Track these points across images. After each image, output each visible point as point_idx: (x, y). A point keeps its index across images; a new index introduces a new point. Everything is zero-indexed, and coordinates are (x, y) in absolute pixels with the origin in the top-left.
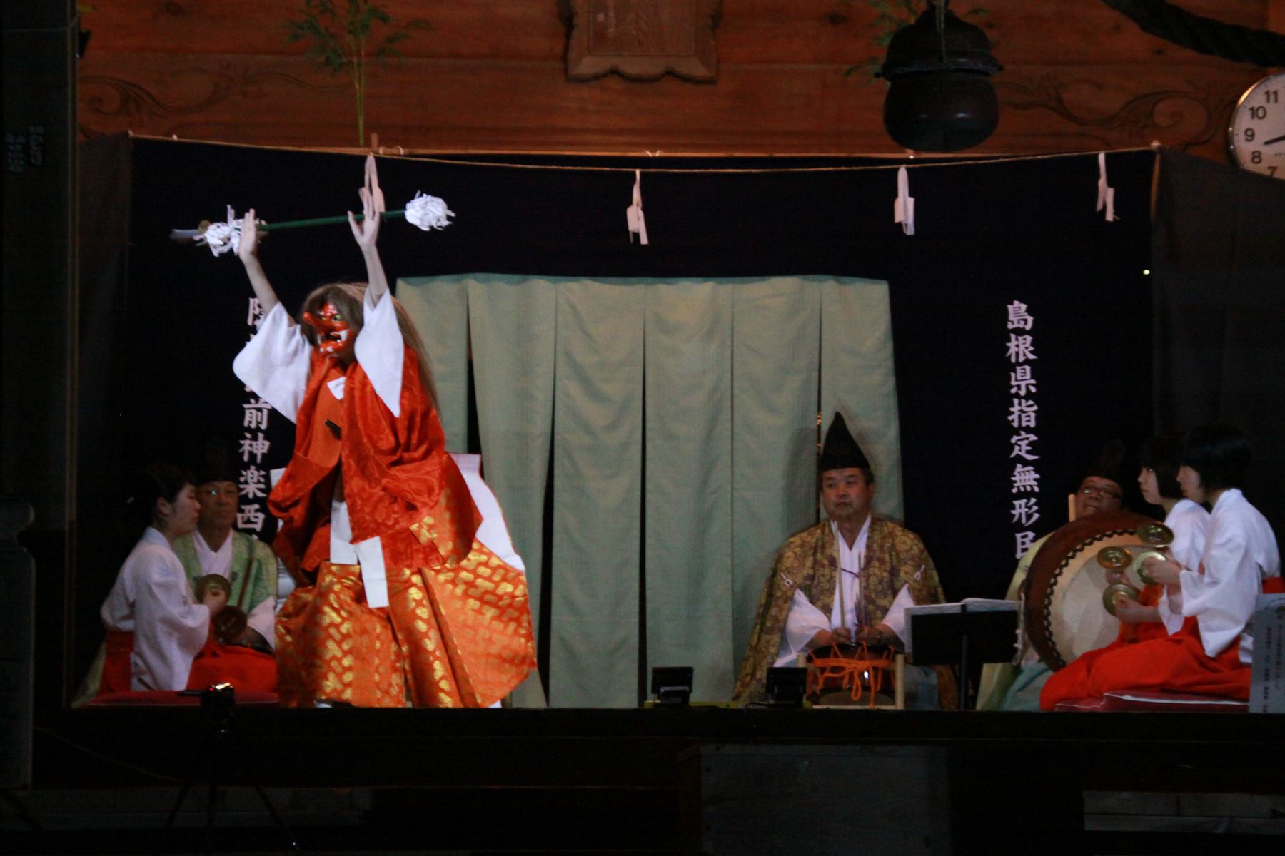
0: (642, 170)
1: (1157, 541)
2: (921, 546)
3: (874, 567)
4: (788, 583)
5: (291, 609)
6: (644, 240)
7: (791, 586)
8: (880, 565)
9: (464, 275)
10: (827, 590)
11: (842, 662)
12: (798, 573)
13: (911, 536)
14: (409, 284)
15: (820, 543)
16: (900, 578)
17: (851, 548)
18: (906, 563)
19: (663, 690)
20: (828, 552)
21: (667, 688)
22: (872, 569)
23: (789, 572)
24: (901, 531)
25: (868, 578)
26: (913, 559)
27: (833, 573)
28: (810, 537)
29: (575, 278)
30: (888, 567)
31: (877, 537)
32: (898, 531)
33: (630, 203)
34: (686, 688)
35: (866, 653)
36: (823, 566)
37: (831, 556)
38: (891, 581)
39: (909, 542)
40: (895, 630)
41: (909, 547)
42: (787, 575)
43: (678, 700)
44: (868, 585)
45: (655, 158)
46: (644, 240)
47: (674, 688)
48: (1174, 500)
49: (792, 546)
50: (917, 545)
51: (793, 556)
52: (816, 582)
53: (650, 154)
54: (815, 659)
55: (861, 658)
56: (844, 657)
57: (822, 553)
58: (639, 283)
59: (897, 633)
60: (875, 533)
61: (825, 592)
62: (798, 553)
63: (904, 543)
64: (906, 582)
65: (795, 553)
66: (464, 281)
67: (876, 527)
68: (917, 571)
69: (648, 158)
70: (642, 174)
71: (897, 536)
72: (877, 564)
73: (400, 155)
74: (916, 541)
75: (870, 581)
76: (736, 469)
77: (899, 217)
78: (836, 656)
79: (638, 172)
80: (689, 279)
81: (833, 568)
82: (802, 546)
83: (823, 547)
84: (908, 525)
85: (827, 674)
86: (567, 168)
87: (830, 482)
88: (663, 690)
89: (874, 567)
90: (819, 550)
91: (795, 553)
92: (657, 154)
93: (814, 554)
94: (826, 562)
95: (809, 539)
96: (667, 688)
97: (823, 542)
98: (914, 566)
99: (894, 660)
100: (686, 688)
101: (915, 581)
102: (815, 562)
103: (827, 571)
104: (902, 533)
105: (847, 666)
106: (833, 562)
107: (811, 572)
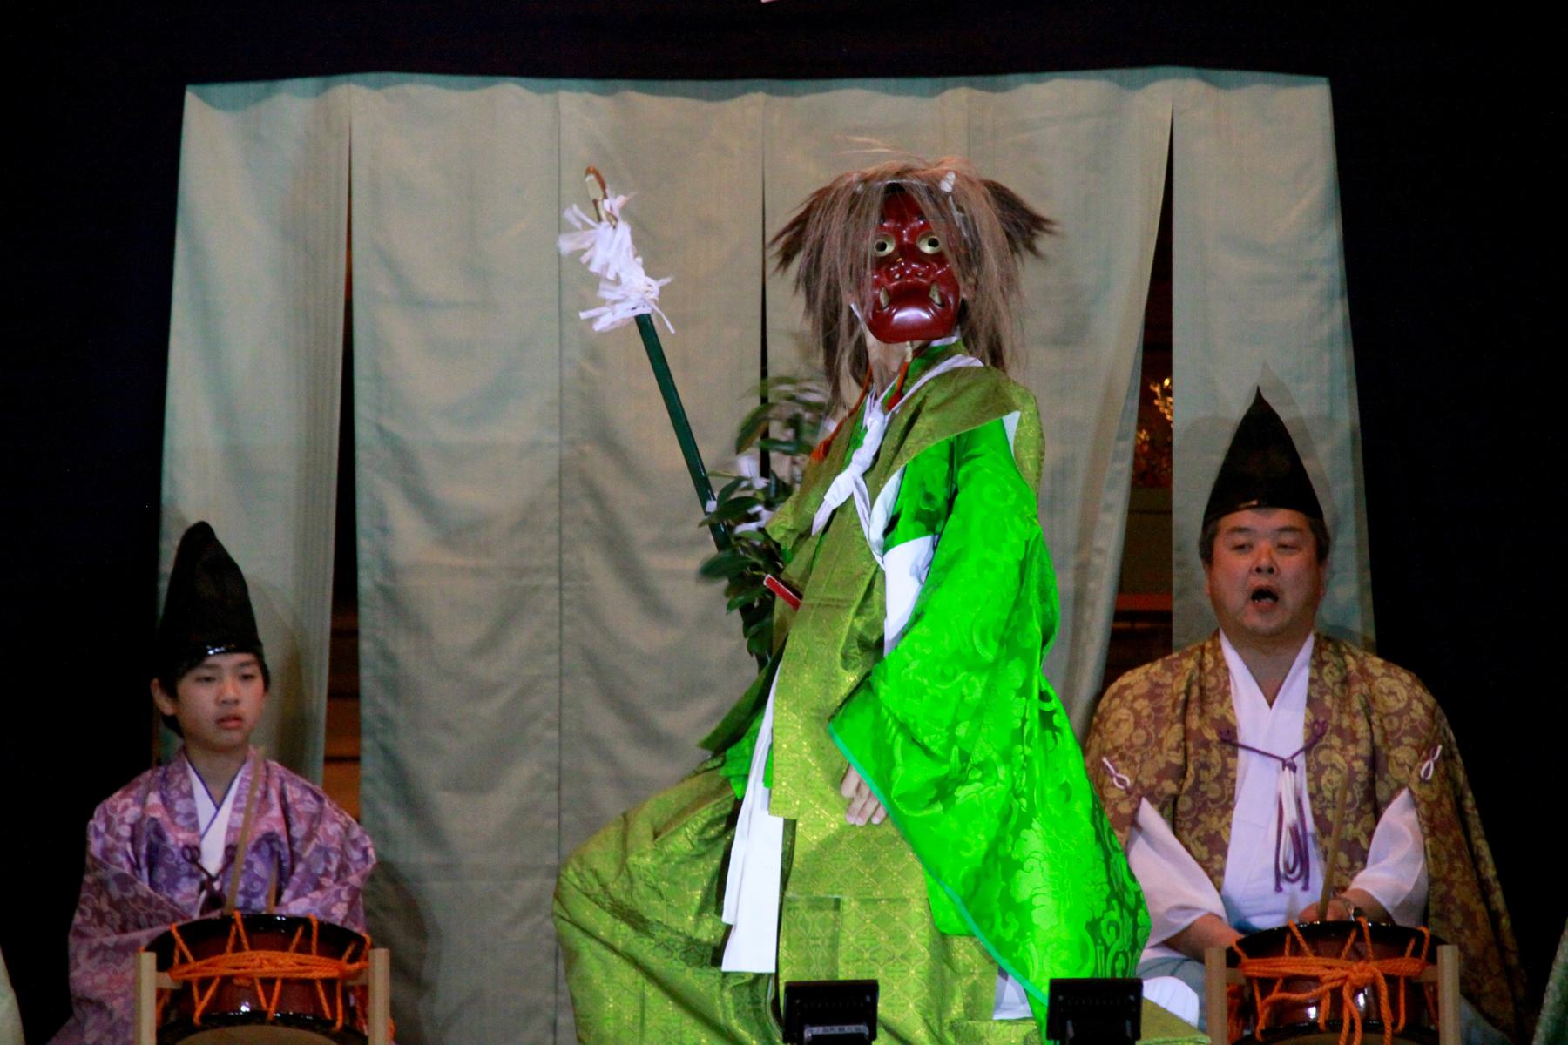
2: (1429, 700)
3: (1331, 747)
4: (1121, 781)
7: (1129, 792)
8: (89, 872)
10: (1213, 801)
11: (1310, 964)
12: (1142, 761)
13: (1406, 677)
15: (1195, 691)
16: (1387, 777)
17: (1271, 705)
18: (1399, 743)
20: (1217, 711)
21: (819, 1030)
22: (1325, 752)
23: (1122, 757)
24: (1383, 665)
25: (1316, 773)
26: (1413, 731)
27: (1230, 760)
28: (1169, 674)
30: (1364, 749)
31: (1330, 677)
32: (1375, 664)
34: (864, 1029)
35: (1368, 946)
36: (1206, 744)
37: (1224, 718)
38: (1372, 781)
39: (1403, 693)
40: (1384, 903)
41: (1402, 705)
42: (1119, 763)
44: (1319, 790)
48: (760, 716)
49: (1128, 695)
50: (1420, 700)
51: (1132, 719)
52: (1189, 782)
54: (1245, 959)
55: (1358, 955)
56: (1317, 954)
57: (1202, 713)
59: (1390, 910)
60: (1326, 670)
61: (1210, 804)
62: (1145, 713)
63: (1392, 693)
64: (1400, 787)
65: (1137, 714)
67: (1325, 656)
68: (1425, 760)
71: (1375, 678)
72: (1336, 741)
74: (1419, 690)
75: (1324, 781)
78: (1297, 951)
81: (1229, 748)
82: (1152, 695)
83: (1203, 698)
84: (1391, 647)
85: (1276, 995)
87: (1241, 539)
89: (1331, 747)
90: (1194, 708)
91: (1137, 714)
93: (1183, 719)
94: (1211, 735)
95: (1168, 679)
96: (819, 1030)
97: (1202, 689)
98: (1419, 750)
99: (1432, 959)
100: (864, 1029)
101: (1423, 781)
102: (1187, 735)
103: (1215, 756)
104: (1383, 670)
105: (1327, 975)
106: (1229, 737)
107: (1176, 759)
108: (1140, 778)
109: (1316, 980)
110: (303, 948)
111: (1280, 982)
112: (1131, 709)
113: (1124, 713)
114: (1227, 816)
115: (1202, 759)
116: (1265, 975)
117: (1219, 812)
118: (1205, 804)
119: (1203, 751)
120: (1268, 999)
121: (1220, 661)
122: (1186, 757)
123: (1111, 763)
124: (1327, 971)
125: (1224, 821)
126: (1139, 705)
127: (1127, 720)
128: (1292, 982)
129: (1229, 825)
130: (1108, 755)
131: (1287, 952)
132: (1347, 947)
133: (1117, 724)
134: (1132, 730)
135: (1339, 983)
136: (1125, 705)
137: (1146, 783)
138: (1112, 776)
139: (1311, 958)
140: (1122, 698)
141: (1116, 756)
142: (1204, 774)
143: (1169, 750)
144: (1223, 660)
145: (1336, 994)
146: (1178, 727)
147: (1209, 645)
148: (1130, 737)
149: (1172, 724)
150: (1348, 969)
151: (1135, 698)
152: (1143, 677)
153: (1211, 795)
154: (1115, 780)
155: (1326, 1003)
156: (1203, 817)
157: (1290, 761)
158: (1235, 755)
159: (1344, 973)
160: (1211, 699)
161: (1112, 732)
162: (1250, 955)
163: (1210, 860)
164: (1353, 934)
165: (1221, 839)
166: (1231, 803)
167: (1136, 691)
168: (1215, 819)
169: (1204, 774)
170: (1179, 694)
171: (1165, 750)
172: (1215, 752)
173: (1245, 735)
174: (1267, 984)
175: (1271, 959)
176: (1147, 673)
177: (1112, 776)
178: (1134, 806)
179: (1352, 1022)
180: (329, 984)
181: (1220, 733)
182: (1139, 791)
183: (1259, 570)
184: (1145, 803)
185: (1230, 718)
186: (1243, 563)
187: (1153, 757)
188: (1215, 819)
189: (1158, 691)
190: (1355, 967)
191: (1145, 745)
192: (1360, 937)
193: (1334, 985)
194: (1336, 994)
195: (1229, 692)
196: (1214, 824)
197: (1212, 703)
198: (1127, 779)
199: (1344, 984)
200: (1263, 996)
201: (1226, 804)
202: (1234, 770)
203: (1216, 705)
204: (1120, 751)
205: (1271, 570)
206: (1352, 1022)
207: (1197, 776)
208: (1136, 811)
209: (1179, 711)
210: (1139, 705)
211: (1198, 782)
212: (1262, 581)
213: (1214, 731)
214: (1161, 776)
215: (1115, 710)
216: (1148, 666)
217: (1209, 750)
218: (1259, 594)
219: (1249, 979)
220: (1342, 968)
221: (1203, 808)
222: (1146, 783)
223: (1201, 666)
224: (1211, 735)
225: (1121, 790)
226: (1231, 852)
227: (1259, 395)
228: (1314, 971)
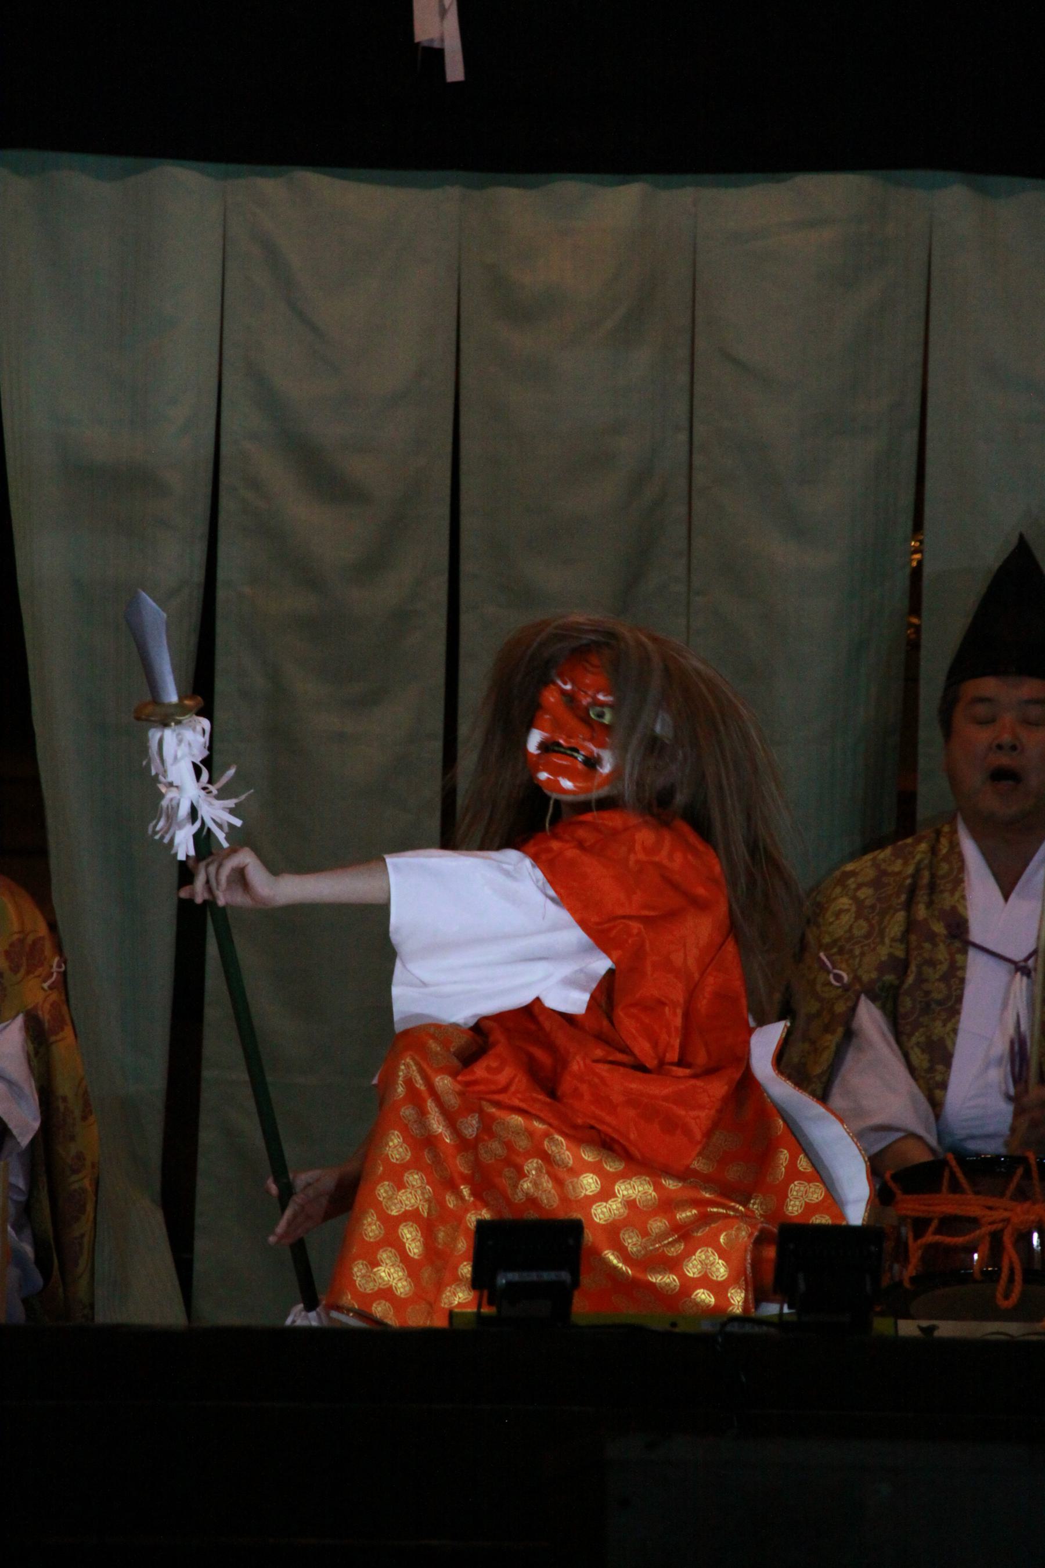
4: (838, 978)
6: (455, 71)
7: (846, 988)
10: (940, 1003)
12: (863, 954)
17: (1006, 897)
20: (947, 901)
21: (514, 1276)
27: (958, 957)
34: (565, 1276)
36: (932, 937)
37: (954, 909)
46: (455, 71)
47: (533, 1276)
49: (851, 882)
51: (854, 909)
54: (899, 1195)
57: (930, 904)
61: (933, 1006)
65: (859, 903)
78: (955, 1187)
81: (958, 944)
82: (876, 883)
83: (932, 887)
85: (930, 1238)
88: (502, 1280)
90: (922, 896)
93: (909, 905)
94: (939, 928)
96: (514, 1276)
97: (933, 876)
100: (565, 1276)
102: (911, 926)
103: (942, 953)
108: (860, 972)
109: (974, 1222)
111: (935, 1223)
112: (854, 898)
113: (845, 902)
114: (953, 1020)
115: (926, 955)
116: (921, 1215)
117: (944, 1015)
118: (928, 1005)
119: (927, 945)
120: (919, 1242)
121: (955, 847)
122: (908, 951)
123: (827, 957)
124: (988, 1212)
125: (949, 1026)
126: (862, 893)
127: (848, 910)
128: (950, 1224)
129: (955, 1031)
130: (827, 948)
131: (944, 1189)
132: (1012, 1186)
133: (838, 914)
134: (853, 920)
135: (1000, 1226)
136: (847, 895)
137: (865, 978)
138: (829, 972)
139: (971, 1196)
140: (844, 886)
141: (835, 950)
142: (927, 970)
143: (893, 940)
144: (958, 844)
145: (996, 1239)
146: (901, 916)
147: (946, 829)
148: (851, 927)
149: (897, 911)
150: (1011, 1210)
151: (860, 886)
152: (869, 864)
153: (936, 996)
154: (831, 977)
155: (985, 1246)
156: (924, 1020)
157: (1022, 964)
158: (965, 952)
159: (1007, 1214)
160: (942, 887)
161: (831, 923)
162: (906, 1191)
163: (931, 1069)
164: (1020, 1171)
165: (945, 1048)
166: (957, 1007)
167: (860, 879)
168: (938, 1024)
169: (927, 970)
170: (905, 879)
171: (887, 941)
172: (942, 947)
173: (976, 934)
174: (920, 1225)
175: (926, 1196)
176: (874, 859)
177: (829, 972)
178: (850, 1004)
179: (1012, 1270)
181: (948, 926)
182: (858, 987)
183: (1000, 747)
184: (863, 998)
185: (960, 909)
186: (983, 737)
187: (874, 949)
188: (938, 1024)
189: (885, 880)
190: (1019, 1209)
191: (867, 936)
192: (1027, 1174)
193: (994, 1227)
194: (996, 1239)
195: (962, 881)
196: (938, 1029)
197: (942, 892)
198: (844, 975)
199: (1006, 1227)
200: (917, 1237)
201: (952, 1007)
202: (963, 968)
203: (946, 895)
204: (839, 944)
205: (1014, 748)
206: (1012, 1270)
207: (919, 973)
208: (853, 1009)
209: (903, 897)
210: (862, 893)
211: (921, 979)
212: (1004, 760)
213: (942, 924)
214: (882, 968)
215: (835, 899)
216: (876, 853)
217: (935, 945)
218: (999, 775)
219: (903, 1219)
220: (1006, 1210)
221: (926, 1009)
222: (865, 978)
223: (934, 850)
224: (939, 928)
225: (838, 987)
226: (956, 1062)
228: (975, 1211)
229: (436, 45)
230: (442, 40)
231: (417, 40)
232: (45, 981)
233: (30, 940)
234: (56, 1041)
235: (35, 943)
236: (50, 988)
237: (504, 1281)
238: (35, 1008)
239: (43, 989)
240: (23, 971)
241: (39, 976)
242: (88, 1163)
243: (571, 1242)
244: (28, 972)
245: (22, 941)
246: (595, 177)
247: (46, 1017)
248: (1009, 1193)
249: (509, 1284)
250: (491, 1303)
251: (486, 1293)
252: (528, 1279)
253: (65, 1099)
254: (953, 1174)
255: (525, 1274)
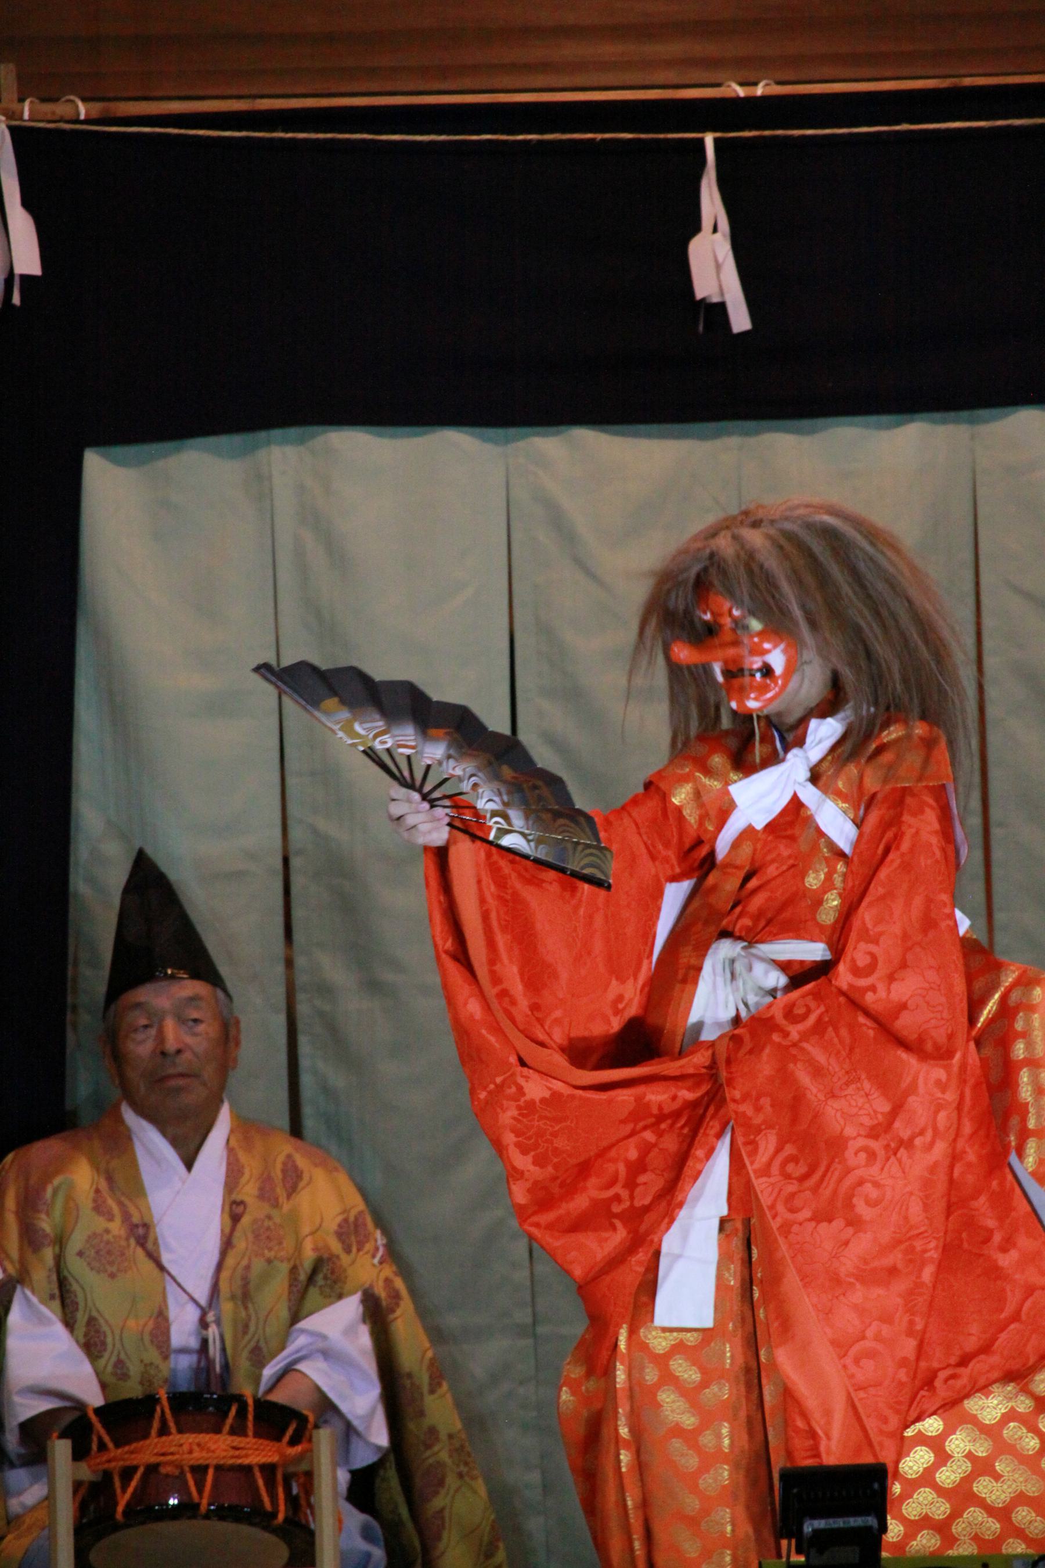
0: (718, 135)
1: (238, 1412)
5: (964, 1155)
6: (740, 320)
9: (262, 435)
14: (118, 462)
19: (809, 1527)
21: (820, 1524)
29: (554, 429)
33: (694, 226)
34: (872, 1521)
43: (850, 1554)
45: (750, 100)
46: (740, 320)
47: (839, 1523)
53: (741, 92)
58: (912, 421)
66: (262, 454)
69: (737, 100)
70: (717, 141)
73: (77, 121)
76: (999, 917)
77: (704, 287)
79: (709, 140)
80: (858, 419)
86: (443, 137)
88: (809, 1527)
92: (759, 91)
96: (820, 1524)
100: (872, 1521)
110: (238, 1430)
132: (229, 1421)
180: (269, 1470)
227: (189, 1165)
229: (716, 299)
230: (722, 293)
231: (699, 294)
232: (374, 1256)
233: (352, 1219)
234: (396, 1319)
235: (356, 1219)
236: (381, 1263)
237: (810, 1529)
238: (371, 1286)
239: (374, 1265)
240: (354, 1249)
241: (367, 1253)
242: (443, 1435)
243: (876, 1486)
244: (359, 1250)
245: (346, 1220)
246: (937, 415)
247: (381, 1292)
248: (227, 1428)
249: (816, 1532)
250: (799, 1552)
251: (793, 1541)
252: (836, 1526)
253: (410, 1375)
254: (163, 1412)
255: (831, 1521)
